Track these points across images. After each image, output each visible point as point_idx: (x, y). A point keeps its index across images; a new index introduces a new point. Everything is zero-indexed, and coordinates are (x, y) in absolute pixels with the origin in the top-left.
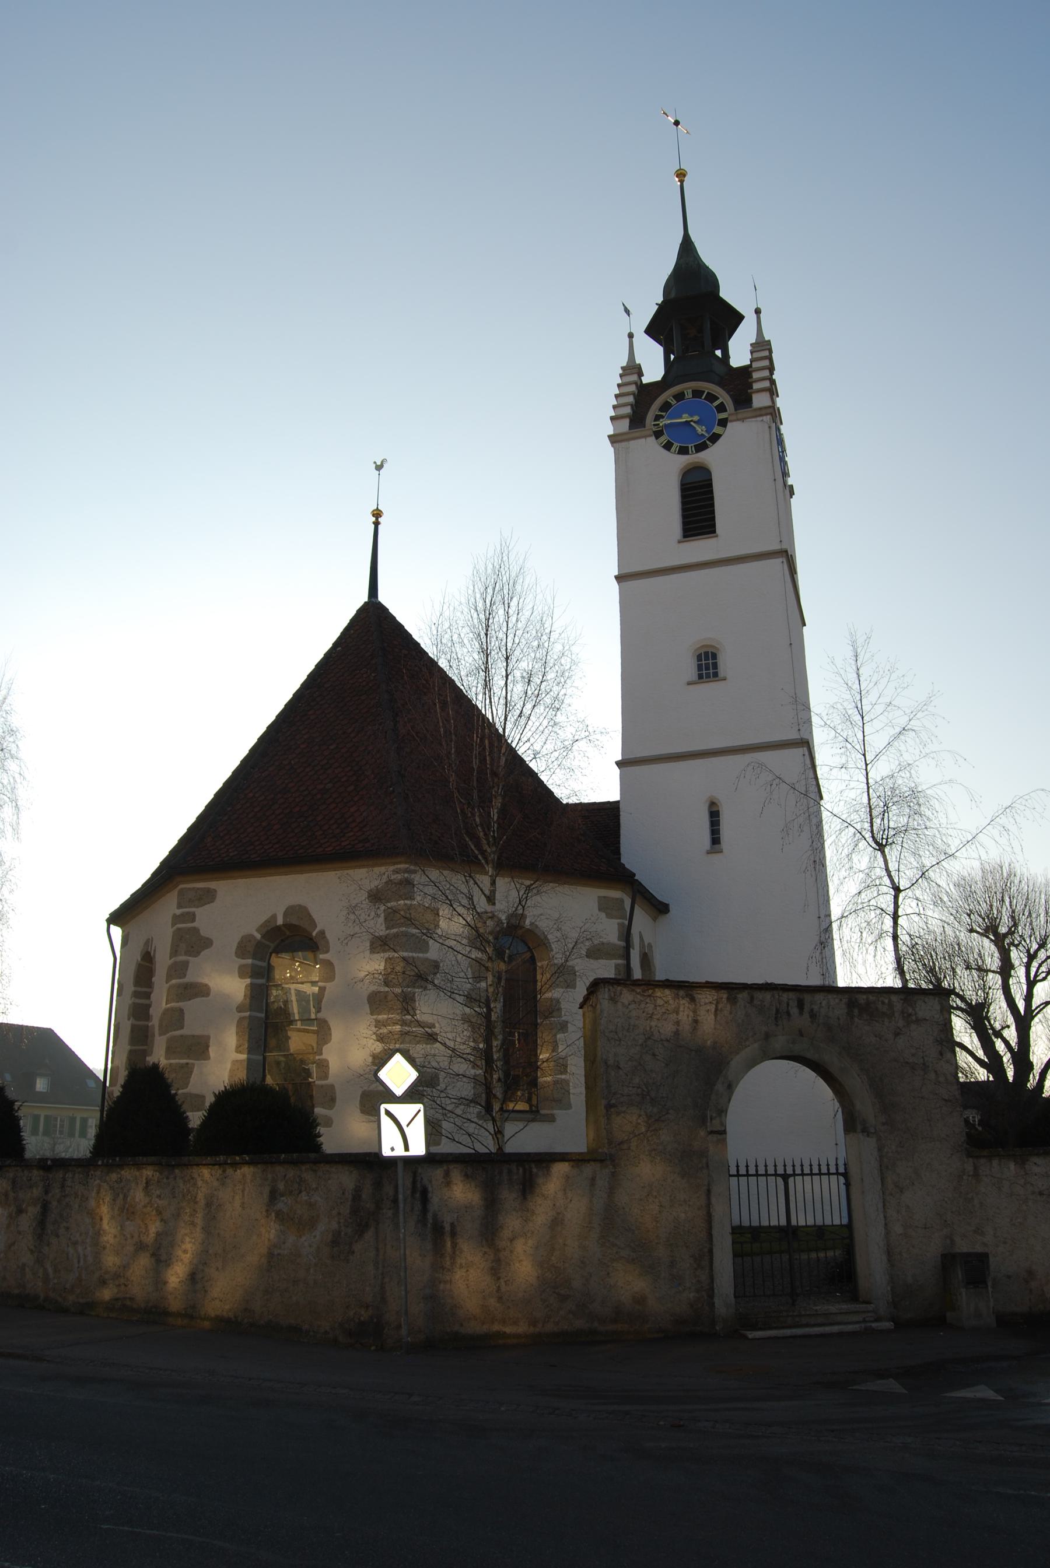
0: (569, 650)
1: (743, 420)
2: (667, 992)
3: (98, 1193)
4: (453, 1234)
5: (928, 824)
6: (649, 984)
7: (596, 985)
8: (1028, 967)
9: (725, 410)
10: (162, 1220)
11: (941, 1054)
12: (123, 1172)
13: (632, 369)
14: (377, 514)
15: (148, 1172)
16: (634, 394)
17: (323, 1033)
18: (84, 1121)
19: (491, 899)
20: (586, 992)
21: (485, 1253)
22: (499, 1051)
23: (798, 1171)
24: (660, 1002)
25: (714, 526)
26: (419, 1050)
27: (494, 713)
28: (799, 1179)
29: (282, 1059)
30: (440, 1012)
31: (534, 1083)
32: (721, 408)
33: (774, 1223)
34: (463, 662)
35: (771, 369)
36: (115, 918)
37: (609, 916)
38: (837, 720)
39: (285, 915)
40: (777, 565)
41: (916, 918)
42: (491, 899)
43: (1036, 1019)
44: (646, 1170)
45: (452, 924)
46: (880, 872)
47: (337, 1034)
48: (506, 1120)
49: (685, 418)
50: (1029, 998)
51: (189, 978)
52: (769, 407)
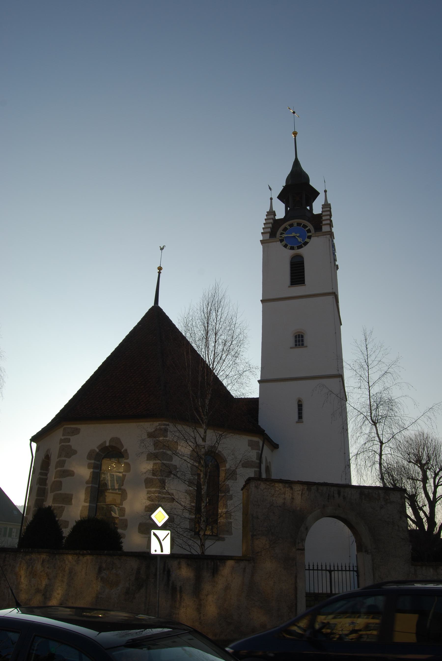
0: (243, 331)
1: (318, 236)
2: (280, 484)
3: (20, 564)
4: (181, 591)
5: (396, 414)
6: (270, 481)
7: (249, 481)
8: (434, 479)
9: (311, 232)
10: (48, 579)
11: (401, 518)
12: (32, 556)
13: (271, 213)
14: (160, 269)
15: (44, 556)
16: (271, 223)
17: (123, 494)
18: (11, 529)
19: (204, 440)
20: (244, 483)
21: (195, 601)
22: (204, 508)
23: (336, 569)
24: (277, 489)
25: (304, 281)
26: (169, 505)
27: (208, 358)
28: (336, 572)
29: (105, 506)
30: (178, 489)
31: (216, 522)
32: (309, 231)
33: (325, 591)
34: (197, 335)
35: (331, 216)
36: (33, 439)
37: (252, 449)
38: (357, 367)
39: (110, 441)
40: (331, 298)
41: (389, 456)
42: (204, 440)
43: (438, 503)
44: (268, 566)
45: (185, 449)
46: (374, 434)
47: (130, 495)
48: (207, 539)
49: (293, 234)
50: (435, 493)
51: (66, 467)
52: (329, 231)
